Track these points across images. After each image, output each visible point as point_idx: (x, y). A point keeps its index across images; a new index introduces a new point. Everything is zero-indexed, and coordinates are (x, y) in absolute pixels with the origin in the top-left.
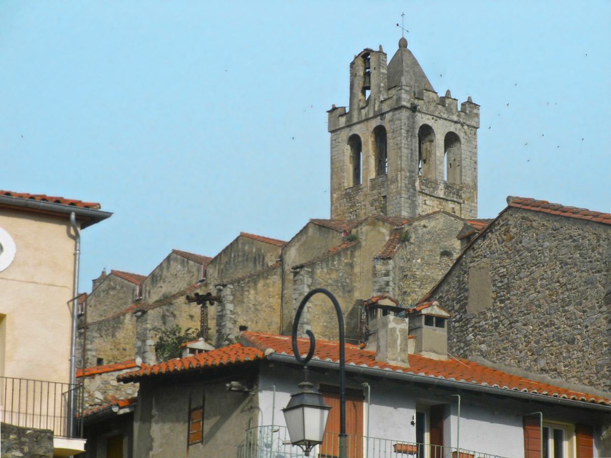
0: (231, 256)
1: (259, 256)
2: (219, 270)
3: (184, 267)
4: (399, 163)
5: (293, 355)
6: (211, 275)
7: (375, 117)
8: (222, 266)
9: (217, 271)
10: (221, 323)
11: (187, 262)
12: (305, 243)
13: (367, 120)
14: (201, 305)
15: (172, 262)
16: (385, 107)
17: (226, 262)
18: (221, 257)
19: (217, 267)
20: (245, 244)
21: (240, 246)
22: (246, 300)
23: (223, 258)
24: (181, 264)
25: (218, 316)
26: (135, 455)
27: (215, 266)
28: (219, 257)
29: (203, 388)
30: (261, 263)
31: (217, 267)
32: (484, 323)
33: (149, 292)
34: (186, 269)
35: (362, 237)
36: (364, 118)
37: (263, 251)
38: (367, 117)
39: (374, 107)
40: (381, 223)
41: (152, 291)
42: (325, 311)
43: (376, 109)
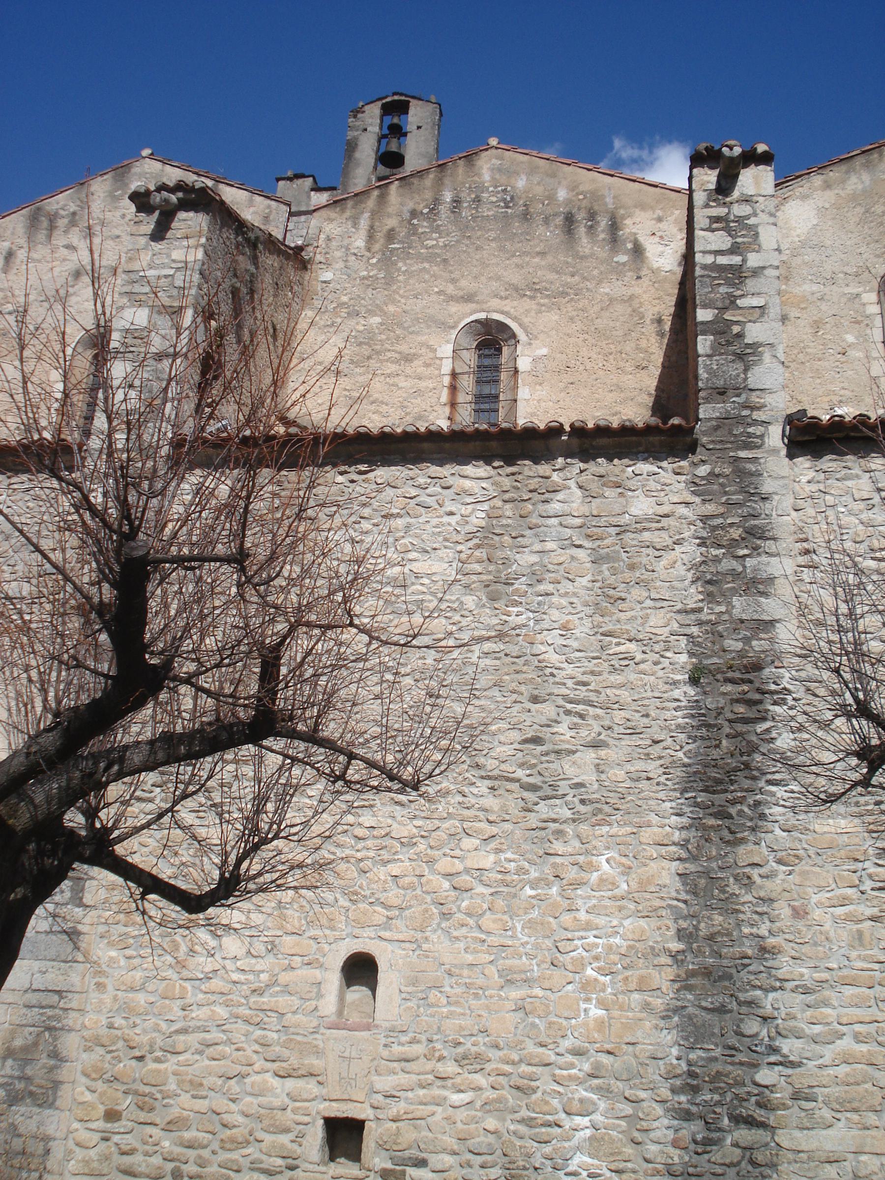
6: (329, 239)
17: (414, 214)
28: (376, 193)
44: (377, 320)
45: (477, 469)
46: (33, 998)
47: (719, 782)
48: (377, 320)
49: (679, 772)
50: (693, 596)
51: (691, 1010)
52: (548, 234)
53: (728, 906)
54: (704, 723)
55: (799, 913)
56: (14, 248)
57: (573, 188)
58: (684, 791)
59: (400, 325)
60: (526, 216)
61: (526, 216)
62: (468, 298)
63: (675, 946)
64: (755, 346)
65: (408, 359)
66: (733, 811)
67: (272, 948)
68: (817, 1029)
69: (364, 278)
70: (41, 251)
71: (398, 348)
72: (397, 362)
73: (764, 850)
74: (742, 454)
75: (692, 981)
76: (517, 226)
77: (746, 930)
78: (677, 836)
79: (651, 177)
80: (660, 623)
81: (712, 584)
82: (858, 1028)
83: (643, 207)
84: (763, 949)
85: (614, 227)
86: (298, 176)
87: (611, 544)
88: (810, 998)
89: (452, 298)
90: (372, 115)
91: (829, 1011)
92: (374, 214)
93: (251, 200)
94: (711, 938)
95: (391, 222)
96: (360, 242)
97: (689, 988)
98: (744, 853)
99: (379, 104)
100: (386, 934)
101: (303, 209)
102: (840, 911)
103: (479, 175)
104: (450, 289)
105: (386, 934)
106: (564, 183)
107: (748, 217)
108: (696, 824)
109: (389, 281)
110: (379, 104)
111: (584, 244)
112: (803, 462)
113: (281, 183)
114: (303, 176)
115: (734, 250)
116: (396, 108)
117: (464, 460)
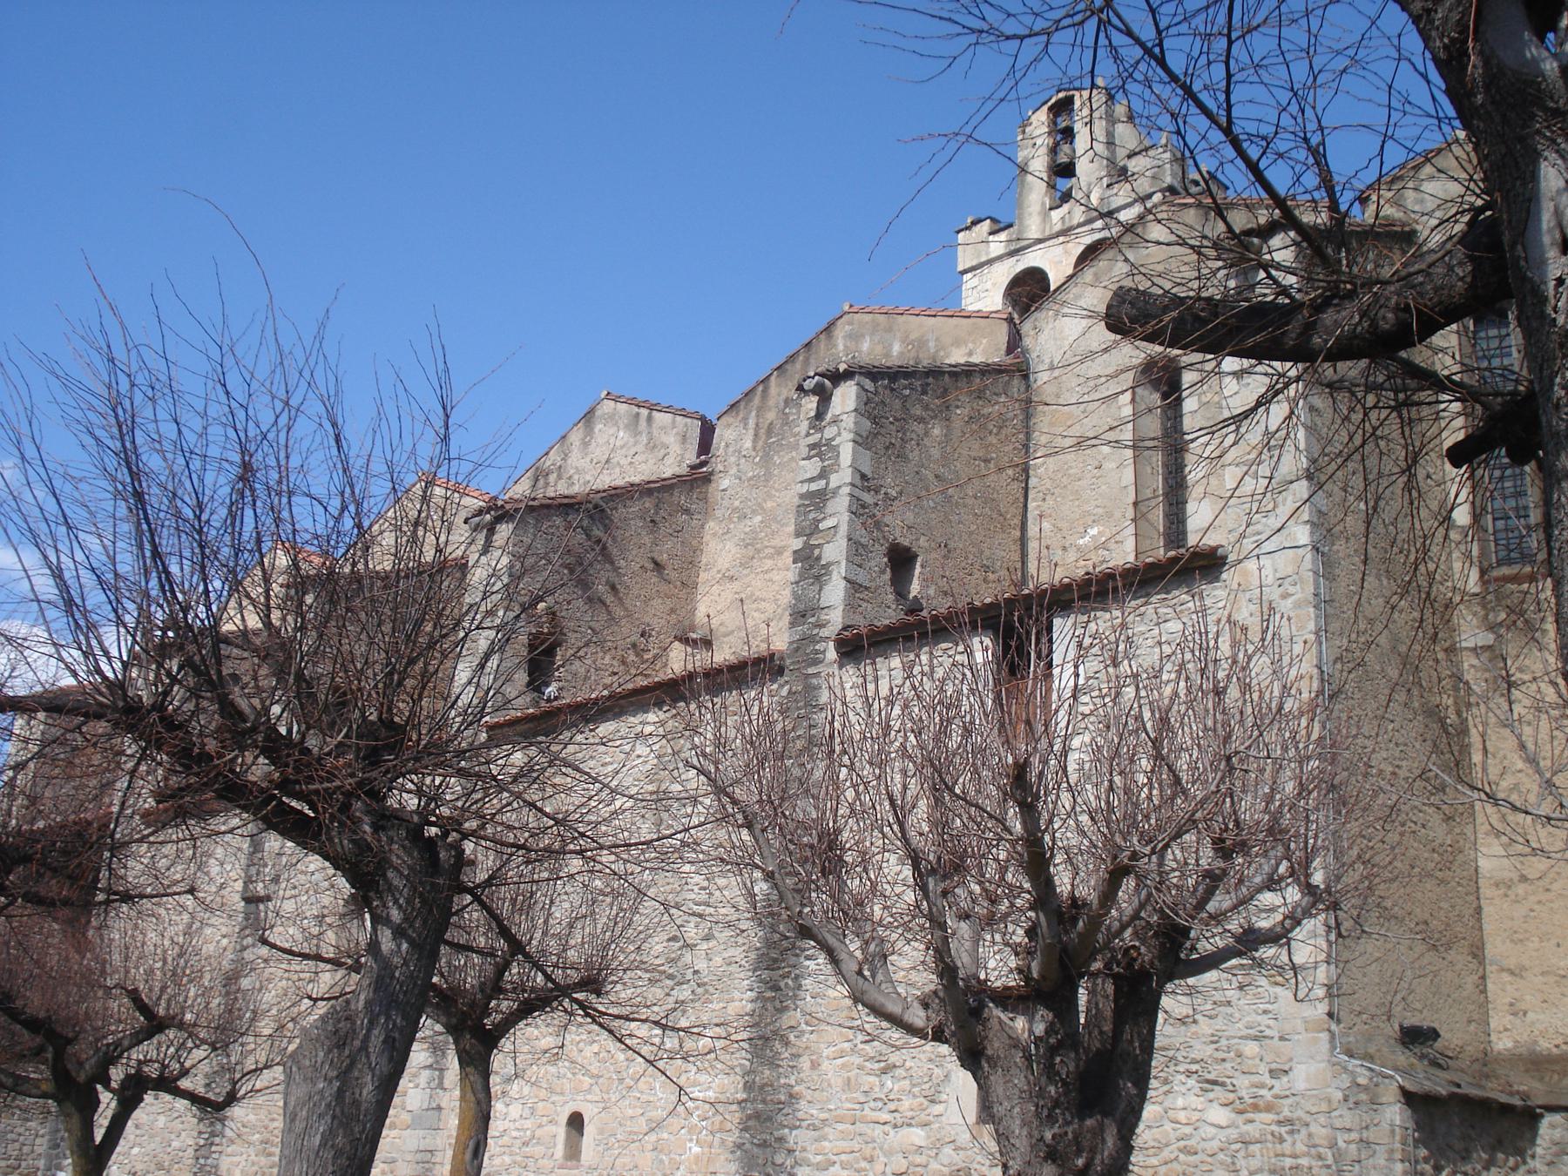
3: (636, 434)
6: (727, 446)
8: (771, 416)
9: (751, 432)
10: (819, 521)
11: (650, 419)
15: (598, 427)
18: (765, 391)
19: (752, 422)
20: (863, 336)
21: (841, 347)
22: (914, 456)
23: (773, 390)
24: (627, 427)
25: (802, 496)
26: (494, 1158)
27: (745, 420)
28: (760, 388)
29: (1256, 1172)
31: (752, 422)
34: (644, 439)
36: (1058, 228)
37: (931, 344)
38: (1067, 225)
42: (1223, 841)
44: (759, 518)
45: (1191, 507)
46: (419, 1156)
47: (775, 960)
48: (759, 518)
49: (753, 956)
51: (748, 1146)
53: (773, 1064)
55: (815, 1065)
58: (755, 970)
59: (775, 519)
63: (741, 1096)
64: (829, 564)
66: (782, 984)
67: (533, 1111)
68: (819, 1158)
69: (751, 479)
71: (773, 543)
72: (771, 557)
73: (798, 1014)
74: (810, 671)
75: (750, 1123)
77: (782, 1081)
78: (750, 1007)
82: (843, 1157)
84: (791, 1096)
86: (974, 223)
88: (816, 1134)
90: (1040, 120)
91: (826, 1144)
92: (759, 409)
93: (674, 422)
94: (762, 1087)
96: (748, 444)
97: (745, 1129)
98: (789, 1018)
99: (1045, 108)
100: (589, 1097)
101: (983, 259)
102: (840, 1061)
103: (835, 346)
105: (589, 1097)
106: (898, 335)
107: (833, 439)
108: (760, 997)
109: (768, 476)
110: (1045, 108)
112: (850, 669)
113: (961, 235)
114: (980, 221)
116: (1063, 107)
117: (645, 709)
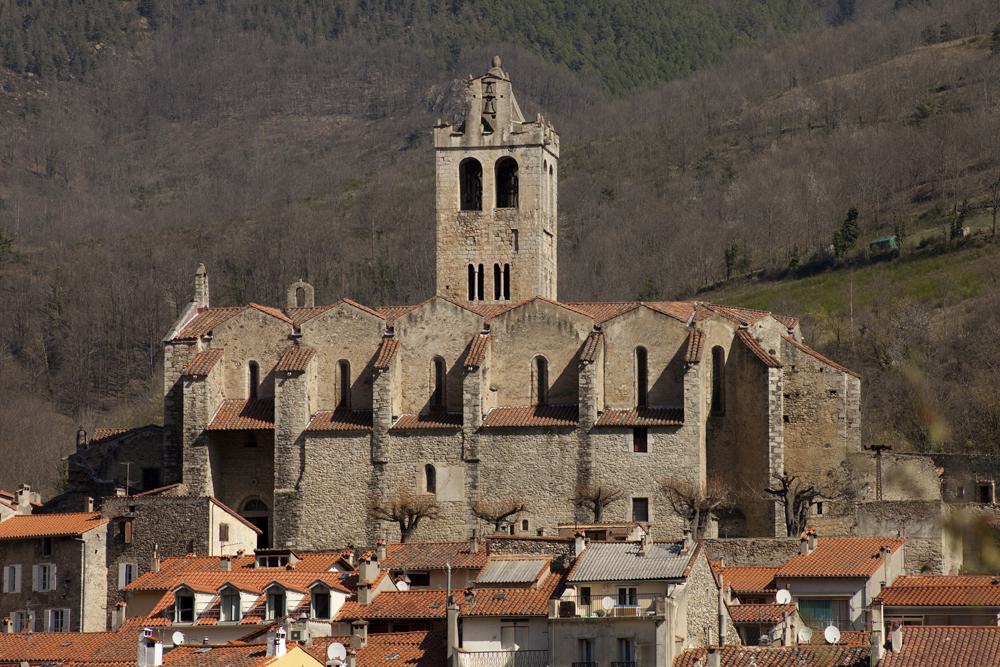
0: (524, 315)
1: (566, 323)
2: (507, 326)
4: (536, 200)
5: (875, 479)
7: (502, 147)
12: (634, 323)
13: (491, 148)
14: (942, 470)
16: (517, 140)
17: (518, 320)
18: (509, 314)
30: (568, 330)
32: (974, 454)
33: (405, 331)
35: (707, 331)
39: (502, 137)
40: (725, 320)
41: (409, 330)
43: (505, 139)
50: (577, 457)
52: (554, 329)
54: (579, 479)
56: (226, 543)
57: (560, 314)
60: (548, 323)
61: (548, 323)
62: (535, 349)
65: (520, 367)
70: (414, 329)
76: (546, 326)
79: (485, 579)
80: (572, 462)
81: (581, 455)
83: (578, 320)
85: (571, 327)
87: (563, 446)
89: (530, 349)
95: (513, 323)
96: (504, 330)
104: (530, 346)
109: (513, 343)
111: (564, 333)
115: (587, 383)
